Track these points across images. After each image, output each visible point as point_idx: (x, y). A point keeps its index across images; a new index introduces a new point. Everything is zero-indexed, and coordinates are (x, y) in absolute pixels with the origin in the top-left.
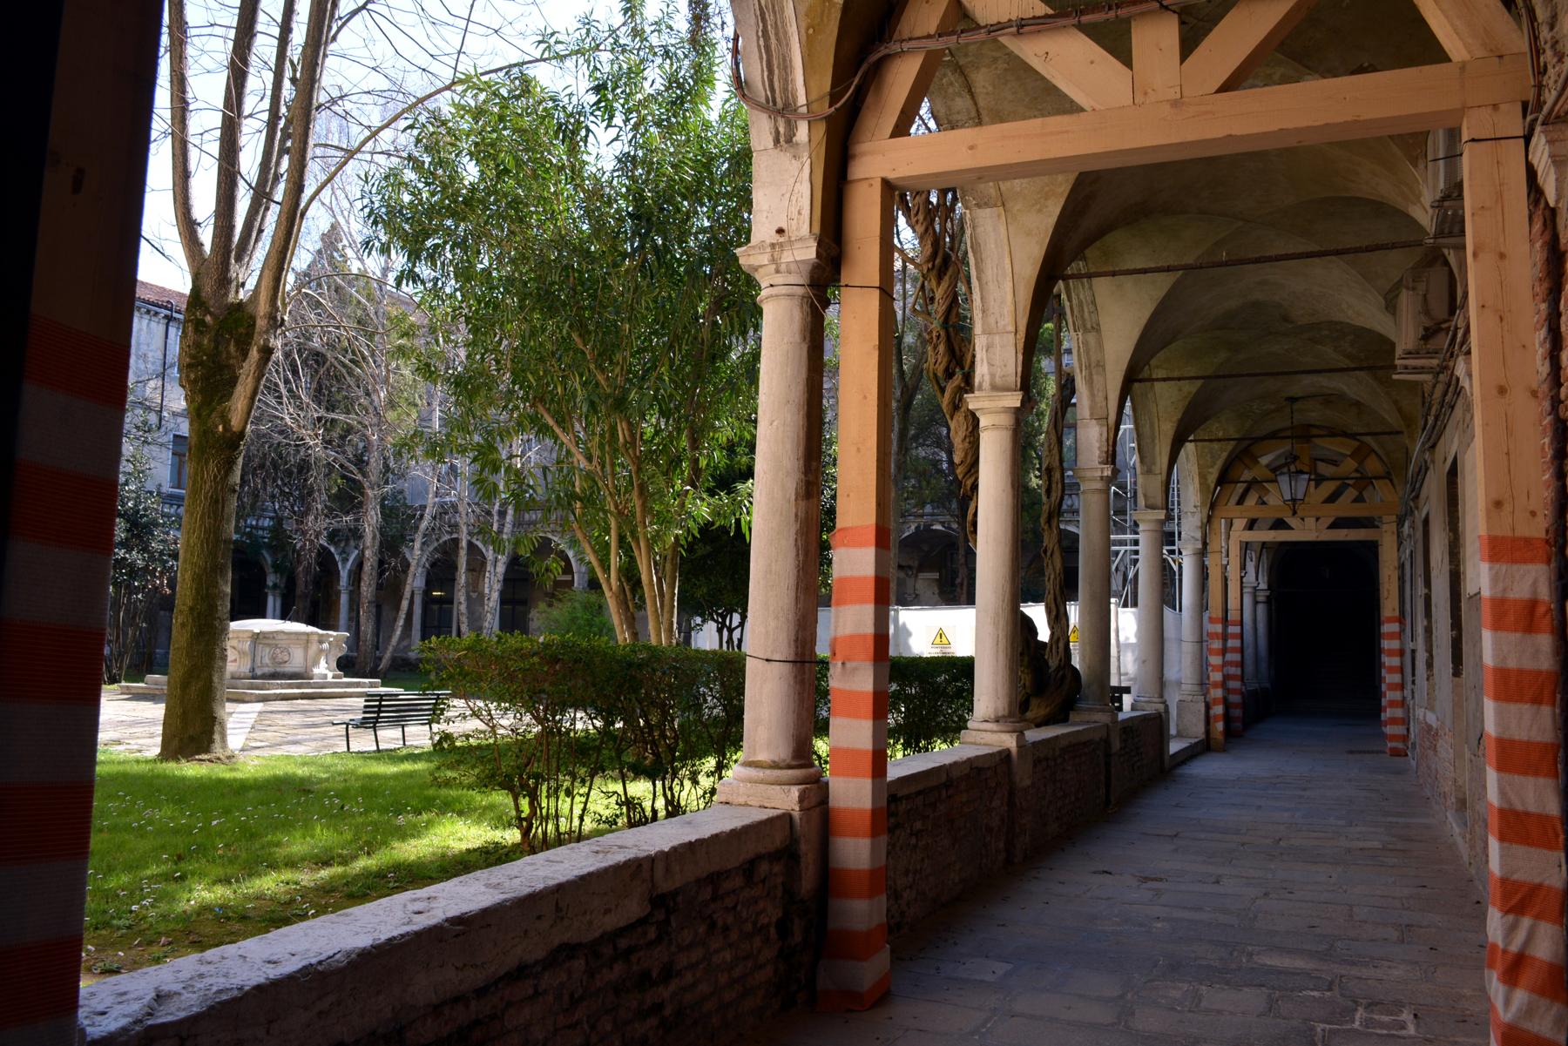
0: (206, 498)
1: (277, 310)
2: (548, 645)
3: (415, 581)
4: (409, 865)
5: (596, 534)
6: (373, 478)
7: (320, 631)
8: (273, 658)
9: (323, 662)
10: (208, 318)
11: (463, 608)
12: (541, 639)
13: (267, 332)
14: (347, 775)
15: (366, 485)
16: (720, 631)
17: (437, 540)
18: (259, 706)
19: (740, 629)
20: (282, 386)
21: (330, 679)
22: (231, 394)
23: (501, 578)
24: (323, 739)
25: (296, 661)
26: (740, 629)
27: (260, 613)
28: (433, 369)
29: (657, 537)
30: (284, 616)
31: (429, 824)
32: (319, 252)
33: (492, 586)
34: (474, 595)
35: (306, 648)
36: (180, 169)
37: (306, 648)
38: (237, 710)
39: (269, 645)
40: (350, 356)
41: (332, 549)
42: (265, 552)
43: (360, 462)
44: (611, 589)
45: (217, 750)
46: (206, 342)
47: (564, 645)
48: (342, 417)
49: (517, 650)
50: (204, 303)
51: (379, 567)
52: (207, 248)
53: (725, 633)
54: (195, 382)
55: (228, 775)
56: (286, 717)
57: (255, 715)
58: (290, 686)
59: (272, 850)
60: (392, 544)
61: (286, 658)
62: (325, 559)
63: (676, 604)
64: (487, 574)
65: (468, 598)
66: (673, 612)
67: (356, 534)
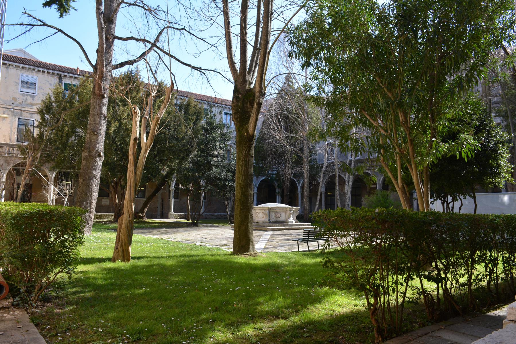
0: (243, 160)
1: (262, 89)
2: (380, 213)
3: (322, 189)
4: (315, 322)
5: (391, 164)
6: (306, 155)
7: (290, 207)
8: (276, 216)
9: (291, 218)
10: (240, 95)
11: (338, 198)
12: (377, 211)
13: (259, 97)
14: (294, 264)
15: (304, 157)
16: (443, 204)
17: (328, 175)
18: (271, 233)
19: (452, 203)
20: (275, 126)
21: (294, 223)
22: (249, 121)
23: (351, 187)
24: (291, 245)
25: (283, 217)
26: (452, 203)
27: (274, 201)
28: (319, 100)
29: (420, 163)
30: (282, 202)
31: (326, 294)
32: (284, 83)
33: (348, 190)
34: (342, 193)
35: (286, 213)
36: (228, 45)
37: (286, 213)
38: (264, 234)
39: (274, 212)
40: (296, 115)
41: (295, 180)
42: (275, 182)
43: (301, 150)
44: (399, 187)
45: (251, 252)
46: (240, 104)
47: (389, 213)
48: (294, 135)
49: (363, 217)
50: (238, 90)
51: (310, 184)
52: (239, 71)
53: (445, 204)
54: (237, 119)
55: (253, 262)
56: (279, 236)
57: (269, 236)
58: (281, 226)
59: (255, 307)
60: (313, 177)
61: (280, 216)
62: (293, 183)
63: (429, 192)
64: (346, 186)
65: (340, 194)
66: (428, 196)
67: (302, 174)
